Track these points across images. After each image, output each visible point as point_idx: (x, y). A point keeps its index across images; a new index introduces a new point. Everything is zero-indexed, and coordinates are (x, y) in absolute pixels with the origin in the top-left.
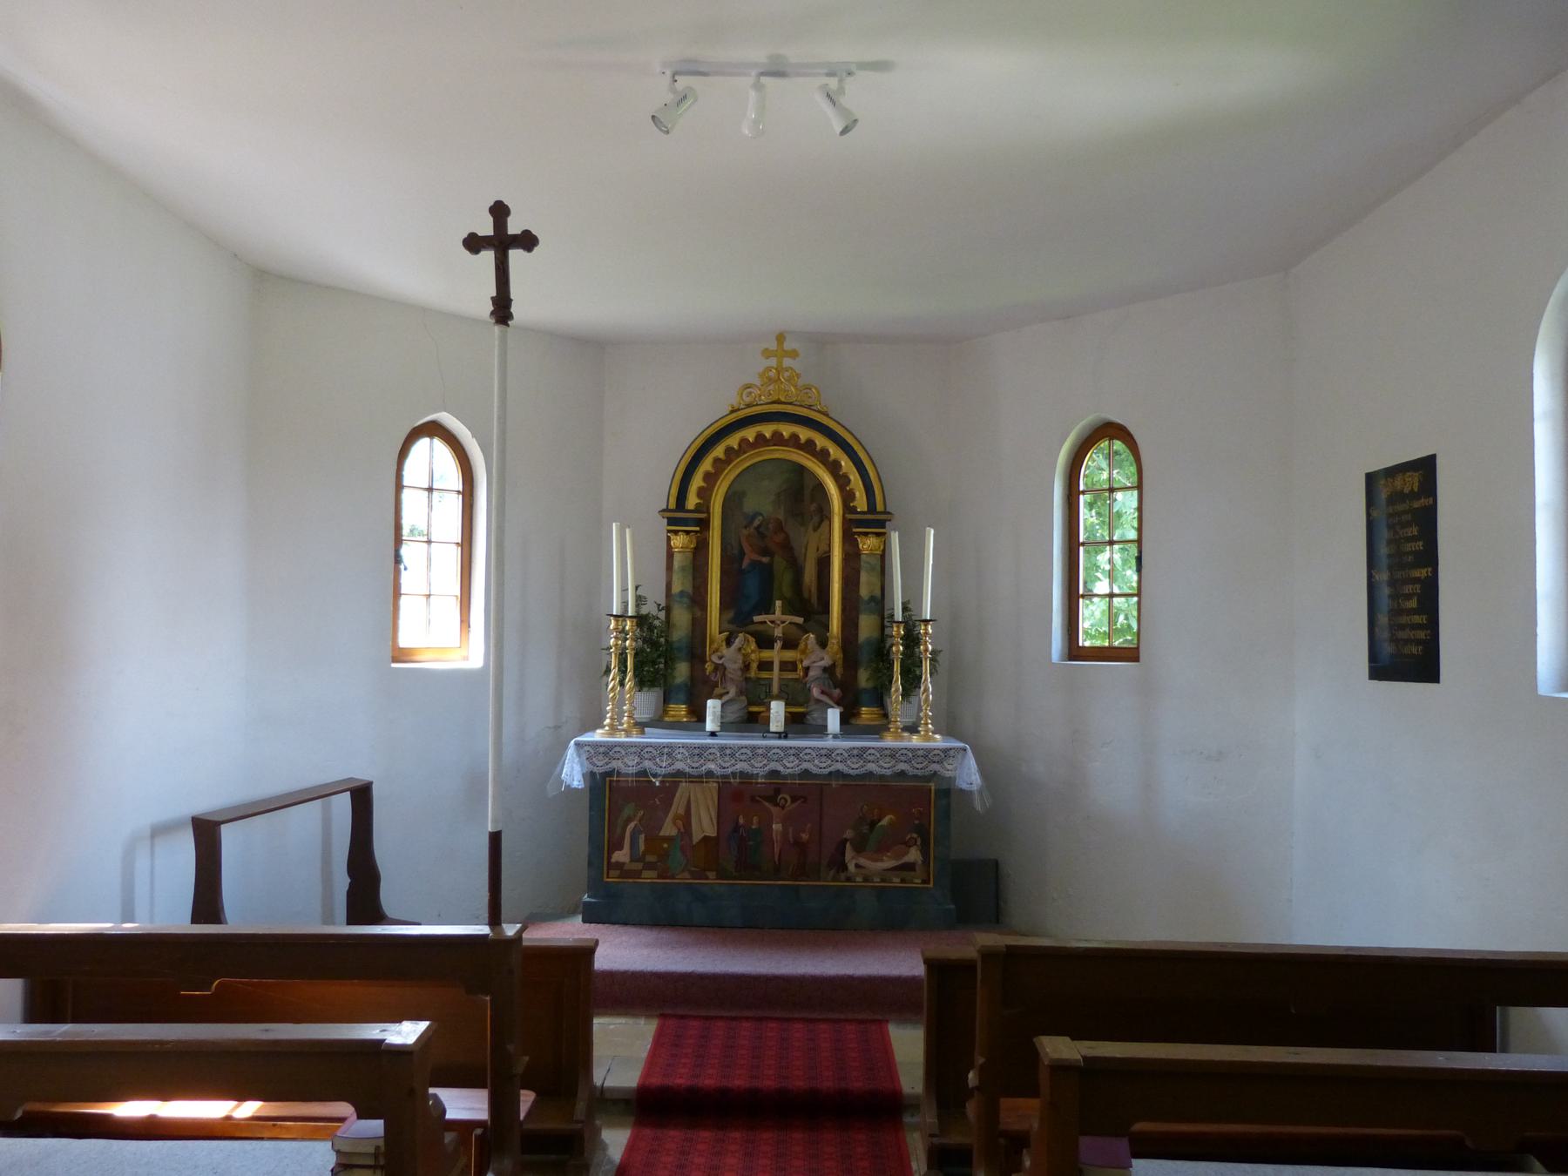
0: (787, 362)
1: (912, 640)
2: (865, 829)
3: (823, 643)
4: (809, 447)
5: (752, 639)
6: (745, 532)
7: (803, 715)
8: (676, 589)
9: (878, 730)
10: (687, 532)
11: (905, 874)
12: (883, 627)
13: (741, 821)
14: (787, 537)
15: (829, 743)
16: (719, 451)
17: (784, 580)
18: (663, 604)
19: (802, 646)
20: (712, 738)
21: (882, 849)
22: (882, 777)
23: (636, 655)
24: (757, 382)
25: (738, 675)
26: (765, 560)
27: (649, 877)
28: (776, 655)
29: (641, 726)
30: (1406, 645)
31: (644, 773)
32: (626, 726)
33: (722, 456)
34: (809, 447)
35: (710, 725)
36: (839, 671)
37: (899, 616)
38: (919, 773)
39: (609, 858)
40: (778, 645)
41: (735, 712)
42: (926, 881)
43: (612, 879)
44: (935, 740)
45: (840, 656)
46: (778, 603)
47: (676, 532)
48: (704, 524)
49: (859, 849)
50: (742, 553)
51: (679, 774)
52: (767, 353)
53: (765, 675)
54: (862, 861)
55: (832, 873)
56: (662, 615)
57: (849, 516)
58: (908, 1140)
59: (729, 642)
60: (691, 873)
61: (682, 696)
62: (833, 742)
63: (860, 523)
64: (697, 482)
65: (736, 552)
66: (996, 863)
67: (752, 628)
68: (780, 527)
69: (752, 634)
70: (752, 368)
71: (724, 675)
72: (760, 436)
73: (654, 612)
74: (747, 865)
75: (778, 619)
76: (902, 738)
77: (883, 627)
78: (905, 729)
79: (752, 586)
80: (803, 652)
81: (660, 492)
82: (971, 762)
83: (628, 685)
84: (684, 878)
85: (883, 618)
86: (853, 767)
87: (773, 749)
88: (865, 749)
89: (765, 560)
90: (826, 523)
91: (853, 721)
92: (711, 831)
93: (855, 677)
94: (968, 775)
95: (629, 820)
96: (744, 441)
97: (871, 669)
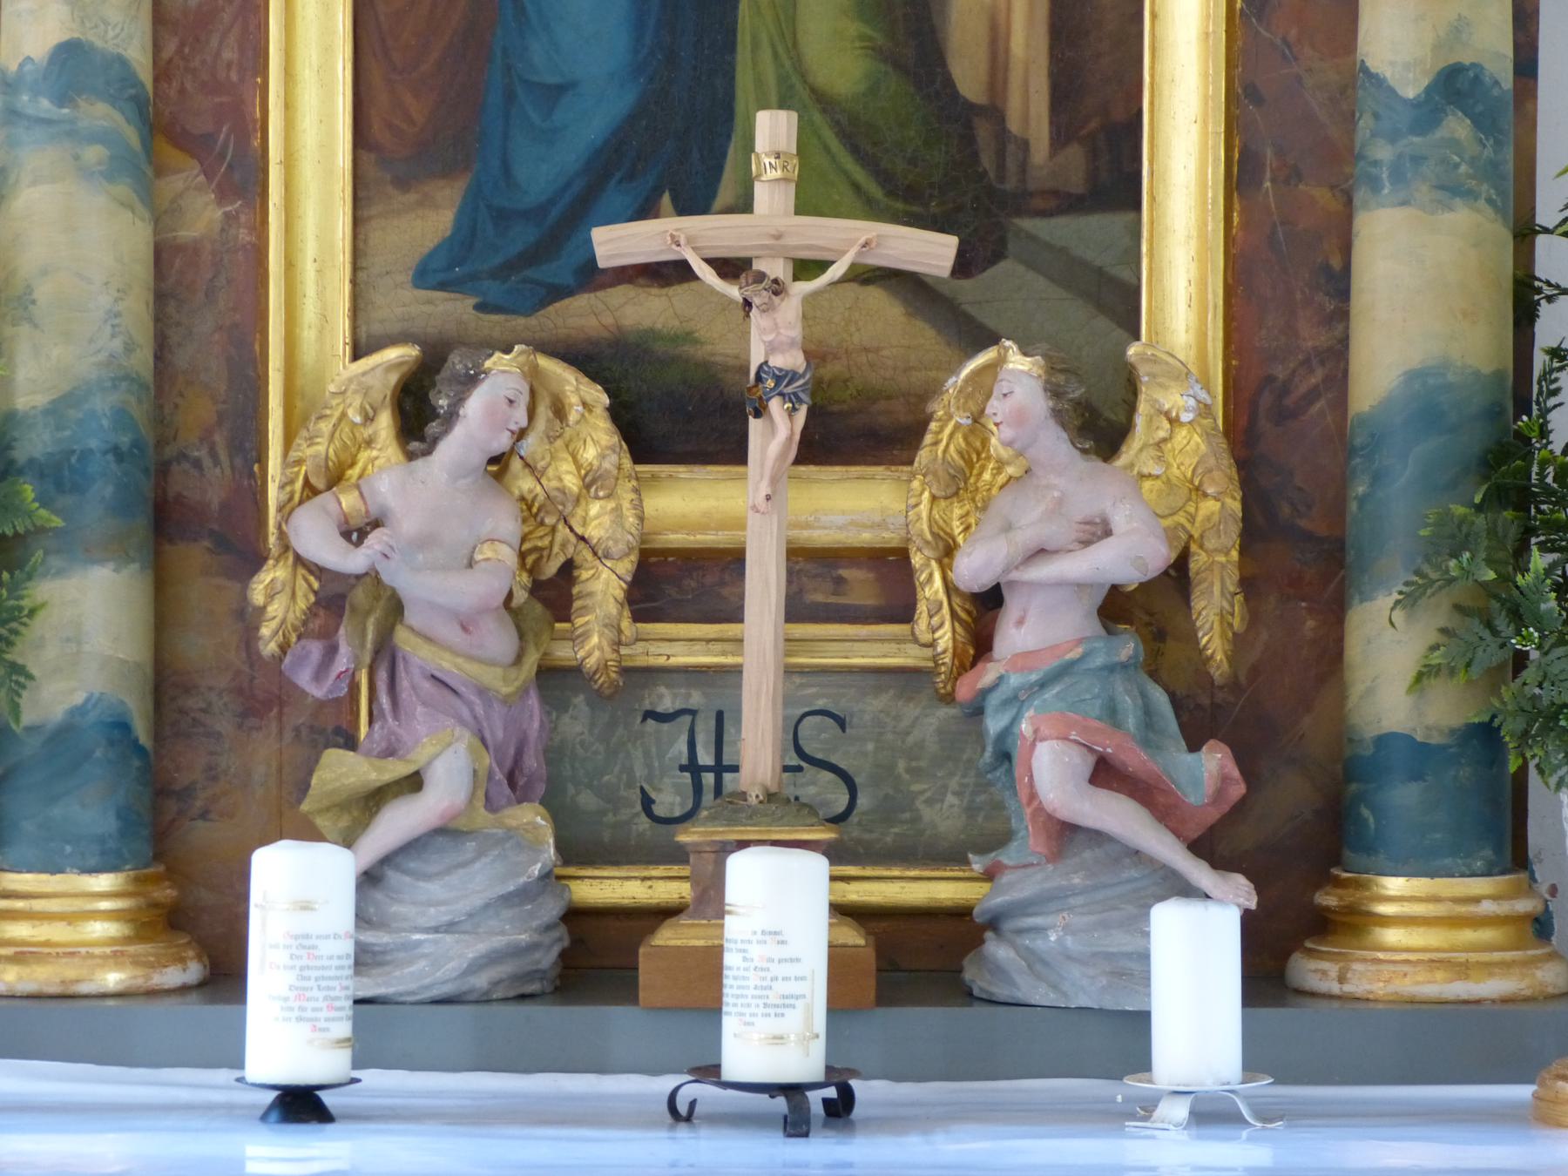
5: (584, 396)
7: (960, 930)
19: (942, 440)
25: (491, 659)
28: (759, 503)
30: (798, 960)
35: (288, 1023)
36: (1214, 616)
40: (774, 434)
41: (468, 920)
45: (1219, 508)
46: (772, 132)
53: (679, 645)
59: (417, 413)
61: (92, 809)
67: (583, 314)
69: (585, 358)
71: (385, 654)
75: (777, 247)
80: (958, 482)
85: (1525, 233)
91: (1313, 971)
93: (1330, 658)
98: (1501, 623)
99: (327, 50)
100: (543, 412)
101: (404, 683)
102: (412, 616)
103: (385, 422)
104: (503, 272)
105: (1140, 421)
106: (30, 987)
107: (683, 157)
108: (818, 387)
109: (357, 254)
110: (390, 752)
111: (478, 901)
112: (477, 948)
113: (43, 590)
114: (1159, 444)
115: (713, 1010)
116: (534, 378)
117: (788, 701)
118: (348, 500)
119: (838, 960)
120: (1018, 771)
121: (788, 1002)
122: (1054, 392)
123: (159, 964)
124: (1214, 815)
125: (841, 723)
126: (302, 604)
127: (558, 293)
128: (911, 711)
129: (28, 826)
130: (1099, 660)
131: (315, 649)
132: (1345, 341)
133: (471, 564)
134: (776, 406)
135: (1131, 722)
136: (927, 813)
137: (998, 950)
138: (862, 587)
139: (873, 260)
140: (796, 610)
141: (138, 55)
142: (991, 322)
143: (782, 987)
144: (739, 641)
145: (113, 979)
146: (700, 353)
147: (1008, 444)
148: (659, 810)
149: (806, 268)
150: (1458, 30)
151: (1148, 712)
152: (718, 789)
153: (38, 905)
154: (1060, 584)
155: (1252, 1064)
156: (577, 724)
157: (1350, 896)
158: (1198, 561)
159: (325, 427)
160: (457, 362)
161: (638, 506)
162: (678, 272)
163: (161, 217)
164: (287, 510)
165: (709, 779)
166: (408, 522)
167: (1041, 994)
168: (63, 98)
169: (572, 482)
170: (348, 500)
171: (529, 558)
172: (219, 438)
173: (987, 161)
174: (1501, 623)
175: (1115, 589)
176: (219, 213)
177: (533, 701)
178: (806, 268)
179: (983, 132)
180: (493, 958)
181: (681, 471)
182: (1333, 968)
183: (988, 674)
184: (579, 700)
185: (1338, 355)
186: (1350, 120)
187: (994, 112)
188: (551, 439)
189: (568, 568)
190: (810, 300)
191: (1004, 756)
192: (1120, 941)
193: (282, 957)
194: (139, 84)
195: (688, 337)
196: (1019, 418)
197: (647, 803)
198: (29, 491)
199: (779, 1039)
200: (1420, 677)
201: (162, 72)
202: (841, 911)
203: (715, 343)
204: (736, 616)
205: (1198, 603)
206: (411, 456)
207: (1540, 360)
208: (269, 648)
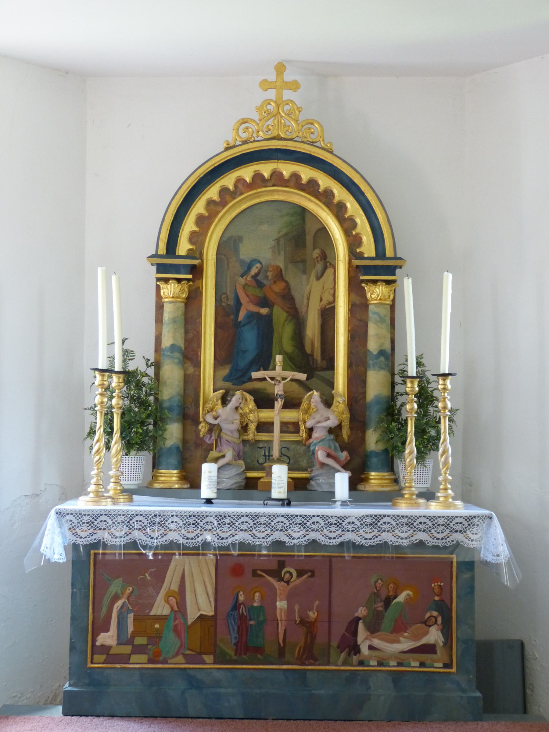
0: (287, 95)
1: (425, 398)
2: (380, 606)
3: (328, 402)
4: (311, 187)
6: (242, 281)
8: (167, 342)
9: (391, 496)
10: (179, 280)
11: (424, 657)
12: (393, 385)
13: (241, 598)
14: (288, 287)
15: (337, 510)
16: (212, 192)
17: (284, 333)
18: (152, 360)
19: (304, 405)
20: (207, 511)
21: (399, 628)
22: (398, 548)
23: (123, 415)
24: (256, 117)
26: (264, 311)
27: (139, 661)
28: (277, 415)
29: (129, 493)
31: (134, 544)
32: (114, 492)
33: (216, 198)
34: (311, 187)
35: (207, 490)
36: (345, 433)
37: (412, 370)
38: (440, 543)
39: (94, 640)
40: (279, 404)
41: (233, 477)
42: (447, 665)
43: (98, 663)
44: (455, 507)
45: (346, 416)
46: (279, 358)
47: (166, 281)
48: (197, 271)
49: (374, 629)
50: (238, 304)
51: (173, 545)
52: (265, 85)
53: (263, 437)
54: (376, 642)
55: (343, 655)
56: (151, 371)
57: (356, 262)
58: (64, 556)
59: (225, 401)
60: (185, 656)
61: (173, 460)
62: (341, 511)
63: (368, 270)
64: (189, 225)
65: (231, 302)
66: (522, 645)
68: (279, 276)
69: (251, 392)
70: (248, 102)
71: (219, 437)
72: (258, 176)
73: (142, 367)
74: (248, 648)
75: (279, 376)
76: (418, 505)
77: (393, 385)
78: (420, 495)
79: (250, 338)
80: (306, 412)
81: (149, 236)
82: (497, 531)
83: (114, 450)
84: (179, 662)
85: (393, 375)
86: (365, 537)
87: (274, 519)
88: (378, 518)
89: (264, 311)
90: (329, 271)
91: (361, 487)
92: (209, 611)
93: (363, 440)
94: (493, 545)
95: (116, 598)
96: (240, 181)
97: (384, 430)
98: (388, 433)
99: (210, 345)
100: (244, 400)
101: (222, 441)
102: (223, 431)
103: (220, 402)
104: (236, 379)
105: (334, 403)
106: (165, 487)
107: (265, 363)
108: (285, 397)
109: (214, 376)
110: (220, 452)
111: (233, 475)
112: (233, 481)
113: (168, 427)
114: (337, 406)
115: (270, 491)
116: (242, 394)
117: (280, 445)
118: (214, 413)
119: (289, 483)
120: (315, 455)
121: (281, 487)
122: (321, 398)
123: (184, 484)
124: (345, 462)
125: (288, 449)
126: (207, 429)
127: (245, 382)
128: (299, 447)
129: (164, 463)
130: (328, 438)
131: (209, 436)
132: (365, 391)
133: (233, 423)
134: (279, 399)
135: (333, 448)
136: (301, 463)
137: (312, 483)
138: (291, 428)
139: (294, 378)
140: (282, 431)
141: (182, 346)
142: (311, 387)
143: (281, 485)
144: (273, 436)
145: (176, 486)
146: (267, 392)
147: (314, 406)
148: (260, 462)
149: (284, 379)
150: (382, 344)
151: (335, 447)
152: (269, 459)
153: (166, 475)
154: (322, 427)
155: (349, 498)
156: (247, 449)
157: (366, 475)
158: (343, 424)
159: (211, 402)
160: (231, 392)
161: (258, 415)
162: (265, 379)
163: (185, 370)
164: (204, 415)
165: (267, 457)
166: (223, 417)
167: (319, 489)
168: (172, 352)
169: (248, 411)
170: (214, 413)
171: (241, 423)
172: (193, 404)
173: (311, 363)
174: (388, 433)
175: (330, 428)
176: (193, 370)
177: (241, 444)
178: (284, 379)
179: (310, 358)
180: (236, 483)
181: (264, 410)
182: (363, 486)
183: (311, 441)
184: (248, 445)
185: (364, 393)
186: (366, 357)
187: (312, 355)
188: (245, 404)
189: (247, 424)
190: (284, 384)
191: (313, 453)
192: (331, 481)
193: (207, 479)
194: (181, 350)
195: (265, 389)
196: (316, 402)
197: (258, 461)
198: (166, 411)
199: (280, 492)
200: (377, 442)
201: (185, 348)
202: (289, 477)
203: (269, 390)
204: (272, 432)
205: (343, 430)
206: (223, 407)
207: (395, 394)
208: (201, 436)
